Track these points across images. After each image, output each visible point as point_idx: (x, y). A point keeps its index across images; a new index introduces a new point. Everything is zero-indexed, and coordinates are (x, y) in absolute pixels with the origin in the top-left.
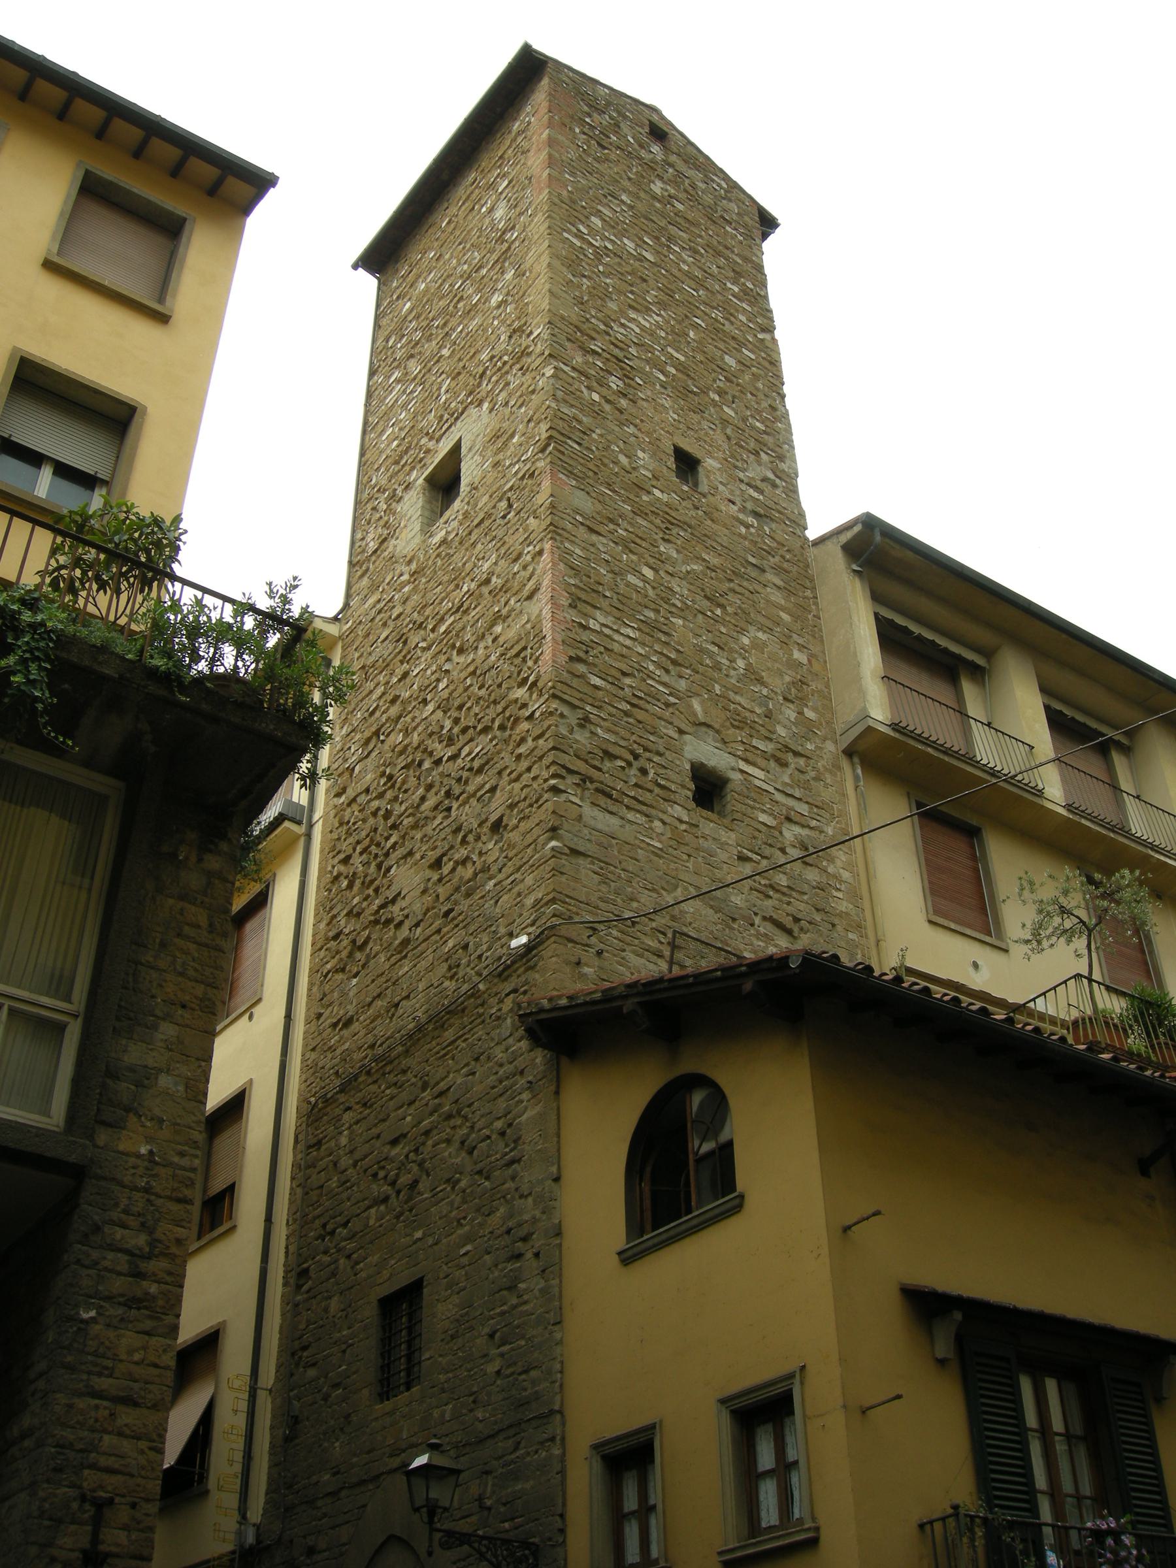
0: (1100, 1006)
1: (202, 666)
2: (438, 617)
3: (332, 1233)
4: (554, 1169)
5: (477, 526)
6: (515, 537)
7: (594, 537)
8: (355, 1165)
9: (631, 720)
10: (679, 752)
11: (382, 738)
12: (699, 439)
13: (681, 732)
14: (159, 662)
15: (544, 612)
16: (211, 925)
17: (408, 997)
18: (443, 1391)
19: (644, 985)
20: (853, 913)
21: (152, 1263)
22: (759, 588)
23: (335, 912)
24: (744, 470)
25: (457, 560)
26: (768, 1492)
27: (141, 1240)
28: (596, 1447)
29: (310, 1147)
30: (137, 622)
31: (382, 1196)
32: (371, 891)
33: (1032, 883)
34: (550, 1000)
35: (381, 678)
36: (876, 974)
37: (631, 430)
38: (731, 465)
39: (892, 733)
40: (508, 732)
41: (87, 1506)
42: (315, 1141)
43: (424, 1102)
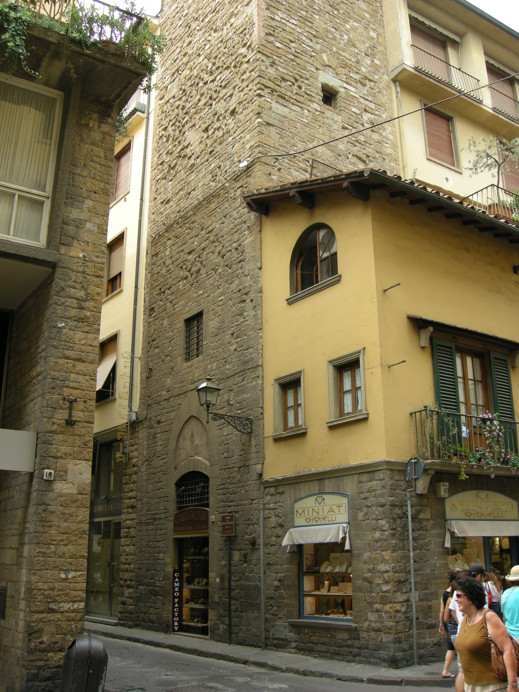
0: (502, 199)
1: (96, 37)
3: (164, 292)
4: (259, 264)
8: (173, 263)
9: (294, 63)
10: (316, 79)
11: (180, 72)
13: (317, 69)
14: (75, 35)
16: (105, 156)
17: (194, 190)
19: (299, 183)
20: (393, 154)
21: (87, 303)
23: (161, 152)
26: (348, 399)
28: (276, 380)
29: (153, 256)
30: (64, 16)
32: (177, 143)
33: (474, 143)
34: (257, 190)
35: (179, 44)
36: (403, 180)
39: (414, 72)
40: (238, 69)
41: (66, 402)
42: (155, 253)
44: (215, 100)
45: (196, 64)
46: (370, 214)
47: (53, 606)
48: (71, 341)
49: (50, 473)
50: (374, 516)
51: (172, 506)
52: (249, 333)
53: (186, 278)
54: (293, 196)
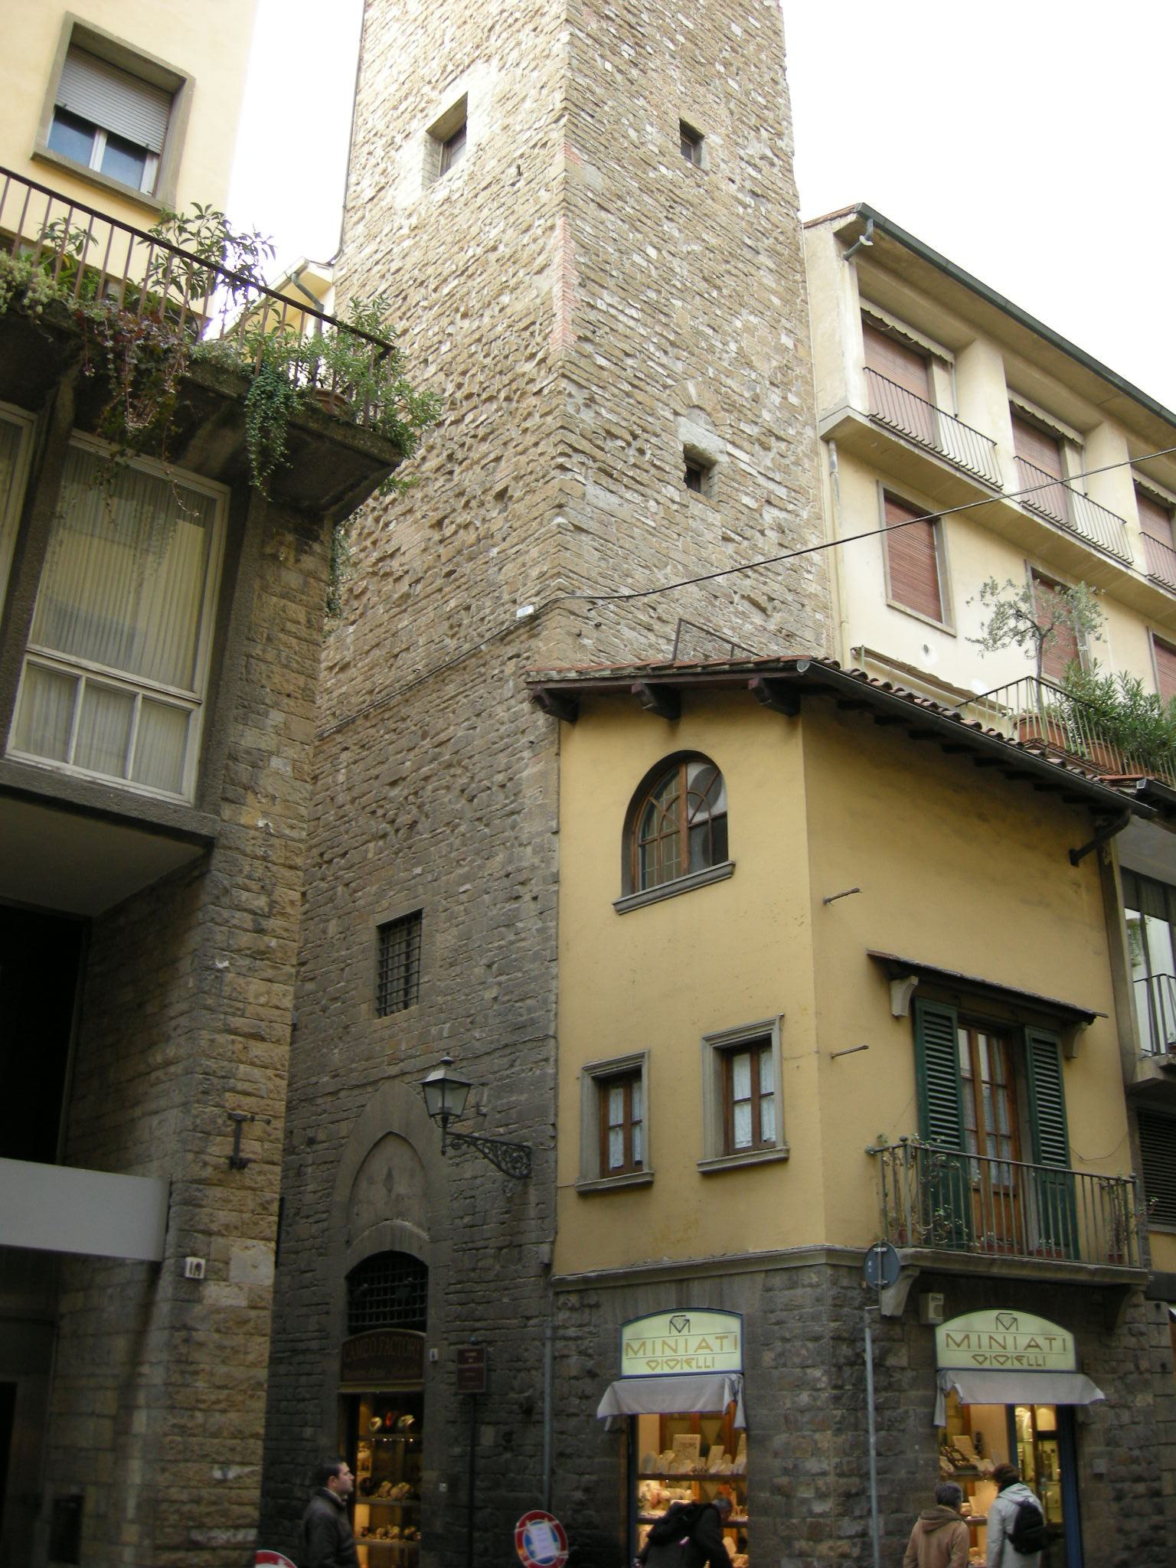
2: (441, 278)
3: (330, 862)
4: (554, 824)
5: (485, 188)
6: (526, 206)
7: (603, 214)
8: (353, 801)
9: (632, 401)
10: (674, 434)
12: (704, 113)
13: (676, 414)
15: (555, 290)
16: (309, 621)
17: (408, 649)
18: (441, 1011)
19: (654, 669)
21: (272, 921)
22: (753, 271)
24: (744, 148)
25: (462, 222)
27: (262, 902)
28: (587, 1069)
31: (381, 833)
32: (368, 543)
34: (560, 672)
37: (641, 102)
38: (733, 141)
40: (514, 405)
43: (423, 750)
44: (461, 463)
45: (418, 380)
46: (800, 743)
47: (197, 1536)
48: (240, 998)
49: (198, 1266)
50: (797, 1360)
51: (337, 1325)
52: (528, 966)
53: (384, 836)
54: (639, 694)
